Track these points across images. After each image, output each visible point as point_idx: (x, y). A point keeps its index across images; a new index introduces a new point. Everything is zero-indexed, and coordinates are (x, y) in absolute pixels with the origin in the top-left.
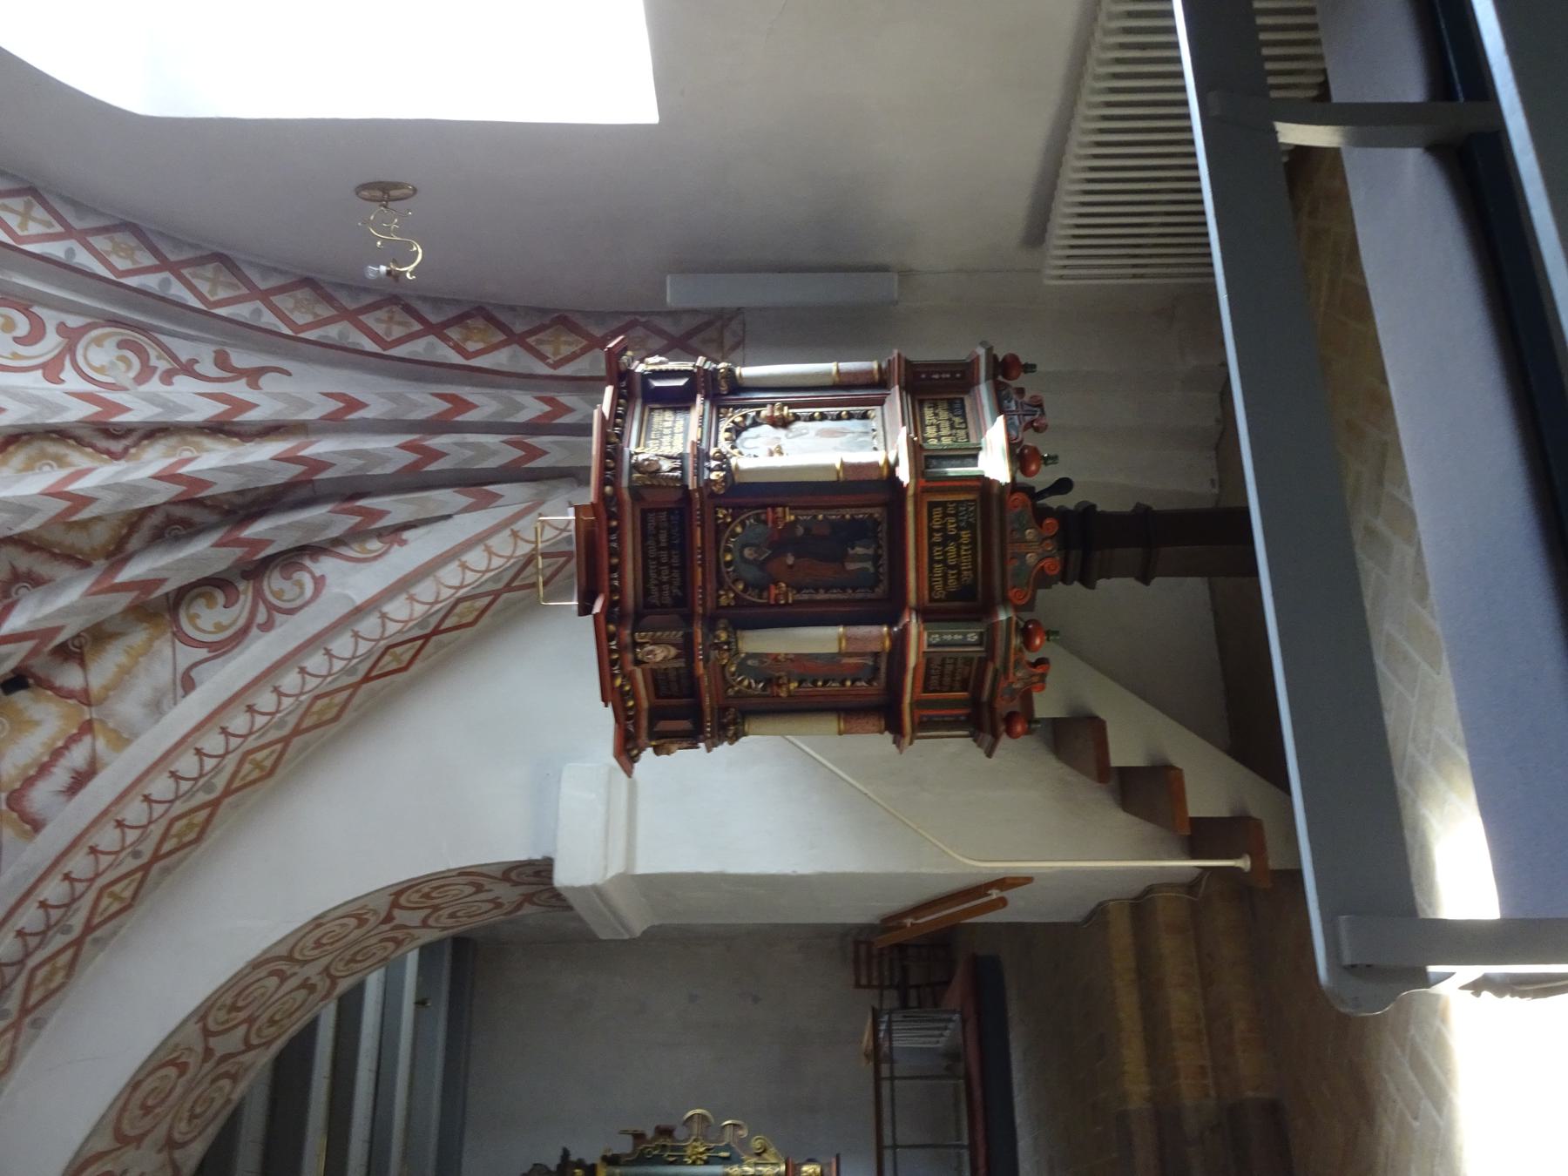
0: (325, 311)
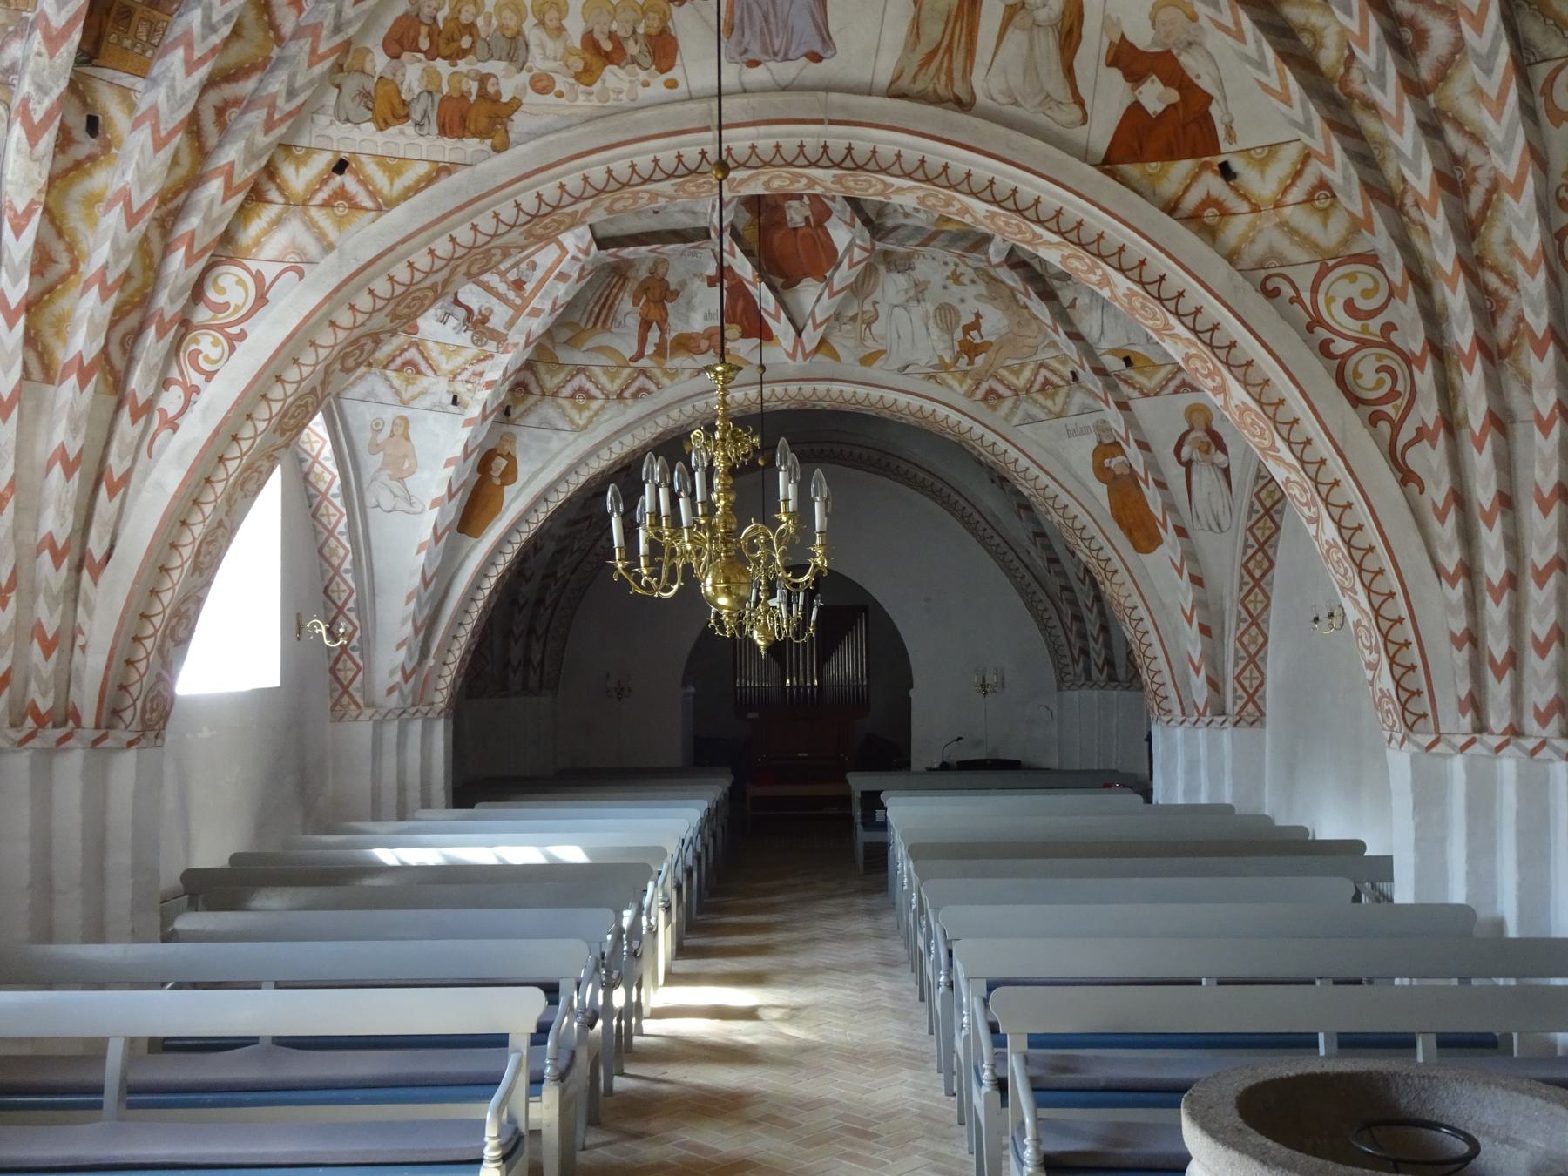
0: (333, 542)
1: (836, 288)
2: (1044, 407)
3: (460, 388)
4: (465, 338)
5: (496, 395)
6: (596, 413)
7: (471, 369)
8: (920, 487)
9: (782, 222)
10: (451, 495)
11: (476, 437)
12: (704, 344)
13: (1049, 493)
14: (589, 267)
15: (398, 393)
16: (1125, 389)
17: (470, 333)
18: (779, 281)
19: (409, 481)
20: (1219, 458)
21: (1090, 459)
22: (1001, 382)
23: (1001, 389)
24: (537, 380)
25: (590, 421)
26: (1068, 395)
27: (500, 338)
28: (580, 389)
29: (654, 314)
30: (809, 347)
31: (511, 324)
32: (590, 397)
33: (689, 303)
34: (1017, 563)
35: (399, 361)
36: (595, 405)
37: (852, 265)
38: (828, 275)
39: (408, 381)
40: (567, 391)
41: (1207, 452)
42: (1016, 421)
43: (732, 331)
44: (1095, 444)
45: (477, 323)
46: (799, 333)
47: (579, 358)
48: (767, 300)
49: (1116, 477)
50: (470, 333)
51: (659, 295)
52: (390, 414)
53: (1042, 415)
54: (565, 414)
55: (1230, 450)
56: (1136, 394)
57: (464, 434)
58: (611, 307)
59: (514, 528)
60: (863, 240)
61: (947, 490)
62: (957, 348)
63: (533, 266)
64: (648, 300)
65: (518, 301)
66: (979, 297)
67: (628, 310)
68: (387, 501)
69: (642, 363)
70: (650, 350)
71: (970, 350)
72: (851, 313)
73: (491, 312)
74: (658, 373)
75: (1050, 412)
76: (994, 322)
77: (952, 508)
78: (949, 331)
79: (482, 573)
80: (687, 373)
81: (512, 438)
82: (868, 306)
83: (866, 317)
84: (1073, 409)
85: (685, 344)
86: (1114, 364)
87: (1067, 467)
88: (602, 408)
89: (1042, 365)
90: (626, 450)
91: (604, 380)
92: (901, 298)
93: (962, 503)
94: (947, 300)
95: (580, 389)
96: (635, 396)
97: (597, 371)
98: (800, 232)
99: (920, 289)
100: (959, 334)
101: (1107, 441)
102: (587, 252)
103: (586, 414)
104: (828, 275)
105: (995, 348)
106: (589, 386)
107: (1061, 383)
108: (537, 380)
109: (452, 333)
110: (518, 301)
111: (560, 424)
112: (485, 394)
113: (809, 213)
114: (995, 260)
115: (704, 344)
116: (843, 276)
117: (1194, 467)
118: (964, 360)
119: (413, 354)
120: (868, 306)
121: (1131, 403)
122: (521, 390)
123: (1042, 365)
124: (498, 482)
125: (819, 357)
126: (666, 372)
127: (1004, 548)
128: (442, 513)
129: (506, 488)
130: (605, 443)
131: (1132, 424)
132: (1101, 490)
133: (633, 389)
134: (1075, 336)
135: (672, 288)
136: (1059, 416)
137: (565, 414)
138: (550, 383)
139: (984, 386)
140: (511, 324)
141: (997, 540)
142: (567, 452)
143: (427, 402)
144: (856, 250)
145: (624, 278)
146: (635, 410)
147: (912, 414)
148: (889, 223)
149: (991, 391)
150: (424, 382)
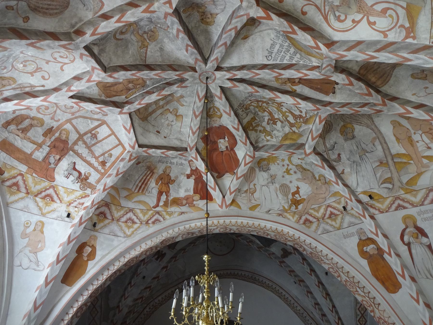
1: (239, 176)
2: (331, 225)
3: (72, 210)
4: (77, 186)
5: (87, 213)
6: (136, 230)
7: (78, 201)
8: (268, 287)
9: (217, 149)
10: (58, 261)
11: (75, 233)
12: (184, 202)
13: (339, 265)
14: (134, 155)
15: (40, 209)
16: (372, 210)
17: (79, 184)
18: (216, 175)
19: (39, 254)
20: (424, 240)
21: (357, 248)
22: (311, 215)
23: (311, 219)
24: (111, 212)
25: (133, 233)
26: (342, 219)
27: (93, 188)
28: (130, 219)
29: (164, 189)
30: (228, 202)
31: (98, 181)
32: (134, 222)
33: (179, 185)
34: (308, 318)
35: (43, 194)
36: (136, 226)
37: (246, 165)
38: (235, 171)
39: (47, 204)
40: (124, 219)
41: (417, 238)
42: (319, 232)
43: (197, 197)
45: (83, 179)
46: (224, 197)
47: (131, 205)
48: (210, 180)
49: (371, 256)
50: (79, 184)
51: (166, 181)
52: (34, 219)
53: (331, 229)
54: (122, 229)
56: (377, 212)
57: (70, 231)
58: (146, 184)
59: (90, 282)
60: (250, 152)
61: (278, 288)
62: (290, 203)
63: (111, 156)
64: (162, 183)
65: (103, 171)
66: (298, 180)
67: (153, 187)
68: (26, 263)
69: (158, 209)
70: (161, 204)
71: (296, 203)
72: (245, 189)
73: (90, 175)
74: (164, 213)
75: (334, 227)
76: (305, 190)
77: (280, 296)
78: (286, 195)
79: (69, 305)
80: (176, 214)
81: (95, 238)
82: (252, 186)
83: (251, 190)
84: (345, 225)
85: (177, 202)
86: (365, 199)
87: (346, 253)
88: (139, 227)
89: (328, 206)
90: (148, 247)
91: (141, 215)
92: (265, 182)
93: (284, 293)
94: (284, 182)
95: (130, 219)
96: (154, 223)
97: (138, 211)
98: (224, 153)
99: (273, 179)
100: (290, 196)
102: (133, 148)
103: (131, 230)
104: (235, 171)
105: (305, 203)
106: (134, 218)
107: (338, 213)
108: (111, 212)
109: (71, 183)
110: (103, 171)
111: (119, 234)
112: (82, 212)
113: (227, 145)
114: (308, 151)
115: (184, 202)
116: (242, 170)
117: (412, 246)
118: (293, 207)
119: (51, 191)
120: (252, 186)
121: (375, 216)
122: (100, 216)
123: (328, 206)
124: (86, 259)
125: (232, 207)
126: (167, 213)
127: (302, 311)
128: (51, 270)
129: (90, 262)
130: (138, 243)
131: (378, 226)
132: (364, 263)
133: (153, 219)
134: (346, 185)
135: (172, 179)
136: (339, 229)
137: (122, 229)
138: (117, 215)
139: (303, 218)
140: (98, 181)
141: (299, 308)
142: (120, 246)
143: (54, 215)
144: (247, 157)
145: (152, 172)
146: (152, 229)
147: (273, 232)
148: (260, 145)
149: (307, 220)
150: (54, 206)
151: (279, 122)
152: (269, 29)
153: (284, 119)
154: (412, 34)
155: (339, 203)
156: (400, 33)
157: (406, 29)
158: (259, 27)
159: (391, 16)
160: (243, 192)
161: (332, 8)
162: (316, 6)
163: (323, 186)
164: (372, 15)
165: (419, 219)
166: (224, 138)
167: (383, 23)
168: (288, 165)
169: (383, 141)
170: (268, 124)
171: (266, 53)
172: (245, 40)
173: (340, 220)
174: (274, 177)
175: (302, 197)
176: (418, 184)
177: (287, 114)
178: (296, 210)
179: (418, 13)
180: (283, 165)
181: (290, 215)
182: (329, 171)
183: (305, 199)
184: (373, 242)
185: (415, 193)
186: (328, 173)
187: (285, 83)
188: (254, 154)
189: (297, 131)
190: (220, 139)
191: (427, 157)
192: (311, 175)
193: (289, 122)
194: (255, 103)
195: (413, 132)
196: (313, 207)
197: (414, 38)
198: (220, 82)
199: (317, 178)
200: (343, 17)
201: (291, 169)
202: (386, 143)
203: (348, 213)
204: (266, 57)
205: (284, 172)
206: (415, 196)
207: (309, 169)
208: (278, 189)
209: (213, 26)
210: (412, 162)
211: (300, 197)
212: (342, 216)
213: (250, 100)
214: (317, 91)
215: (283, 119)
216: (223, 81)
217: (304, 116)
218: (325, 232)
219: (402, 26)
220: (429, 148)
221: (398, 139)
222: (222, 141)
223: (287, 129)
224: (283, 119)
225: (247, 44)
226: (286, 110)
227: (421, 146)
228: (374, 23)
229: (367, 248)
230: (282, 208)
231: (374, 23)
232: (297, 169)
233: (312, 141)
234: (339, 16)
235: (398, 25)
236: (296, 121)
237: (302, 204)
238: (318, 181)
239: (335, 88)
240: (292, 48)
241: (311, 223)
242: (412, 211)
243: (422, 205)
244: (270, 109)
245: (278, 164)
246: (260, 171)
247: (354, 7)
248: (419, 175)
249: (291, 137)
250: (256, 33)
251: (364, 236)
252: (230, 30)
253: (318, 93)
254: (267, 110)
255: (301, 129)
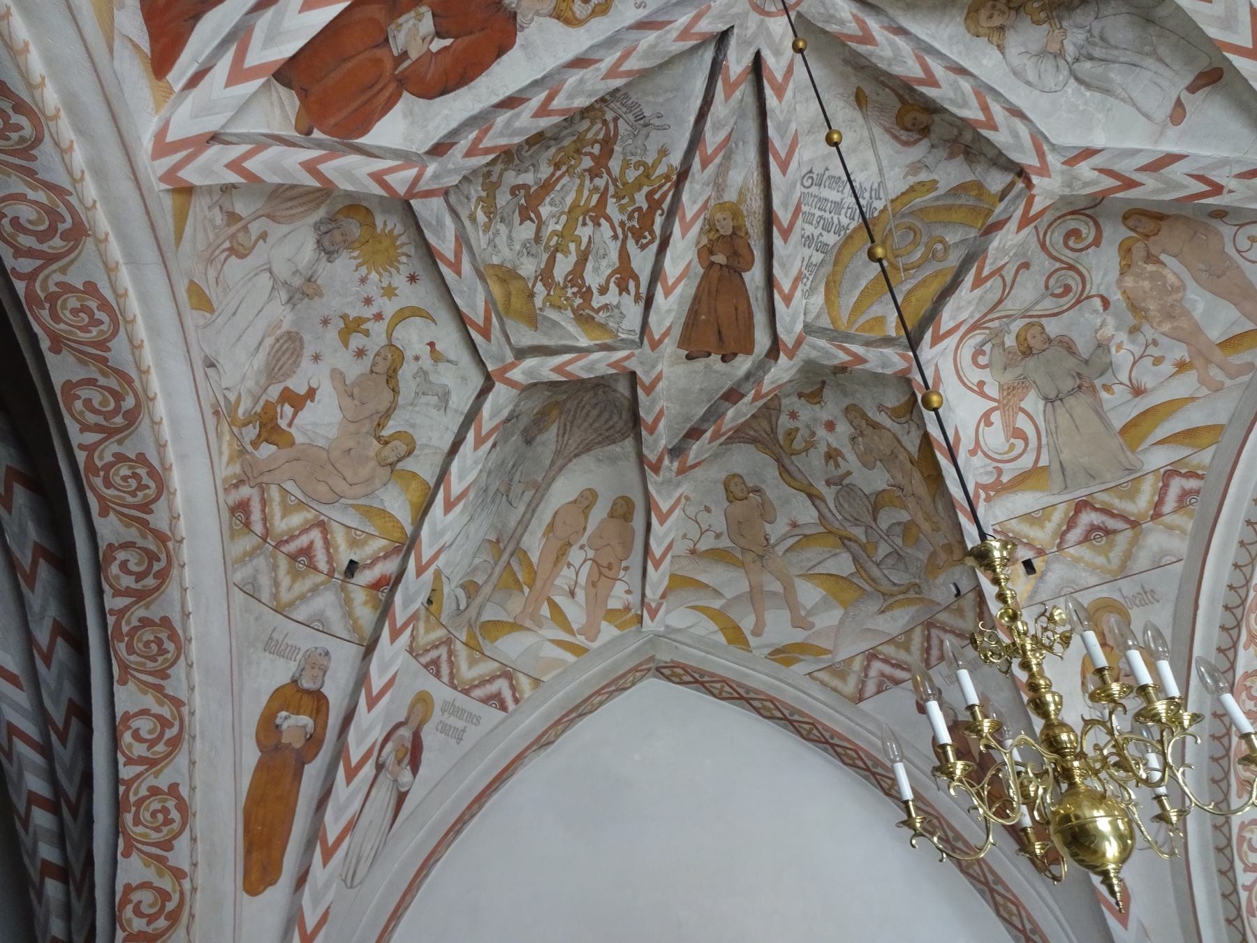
2: (276, 584)
21: (264, 700)
22: (264, 503)
23: (256, 516)
26: (315, 590)
44: (286, 679)
49: (278, 747)
53: (265, 596)
55: (422, 770)
60: (436, 176)
62: (258, 409)
66: (337, 375)
75: (275, 596)
76: (321, 421)
84: (302, 613)
89: (322, 525)
94: (307, 338)
95: (1094, 528)
98: (379, 53)
99: (304, 290)
100: (274, 392)
101: (306, 684)
104: (317, 134)
105: (286, 453)
113: (414, 55)
118: (251, 432)
151: (534, 226)
152: (881, 170)
153: (553, 243)
154: (992, 493)
155: (354, 543)
156: (987, 473)
157: (998, 480)
158: (887, 137)
159: (1012, 447)
160: (227, 206)
161: (997, 335)
162: (1000, 301)
163: (372, 464)
164: (1003, 415)
165: (437, 716)
166: (439, 34)
167: (995, 438)
168: (379, 317)
169: (533, 506)
170: (514, 190)
171: (818, 170)
172: (853, 98)
173: (306, 588)
174: (310, 291)
175: (293, 431)
176: (496, 644)
177: (572, 246)
178: (249, 448)
179: (1034, 489)
180: (368, 301)
181: (230, 444)
182: (476, 462)
183: (293, 444)
184: (318, 711)
185: (477, 655)
186: (469, 462)
187: (710, 231)
188: (429, 194)
189: (538, 302)
190: (434, 15)
191: (553, 606)
192: (383, 407)
193: (552, 261)
194: (597, 134)
195: (584, 540)
196: (289, 486)
197: (988, 499)
198: (749, 32)
199: (386, 433)
200: (982, 360)
201: (367, 333)
202: (534, 511)
203: (343, 589)
204: (811, 171)
205: (344, 317)
206: (472, 663)
207: (402, 390)
208: (279, 332)
209: (962, 29)
210: (526, 590)
211: (290, 425)
212: (322, 583)
213: (616, 120)
214: (688, 317)
215: (550, 239)
216: (750, 44)
217: (595, 305)
218: (249, 588)
219: (1000, 472)
220: (572, 594)
221: (551, 526)
222: (427, 24)
223: (528, 268)
224: (550, 239)
225: (842, 104)
226: (585, 241)
227: (565, 577)
228: (989, 424)
229: (286, 718)
230: (232, 397)
231: (989, 424)
232: (377, 354)
233: (552, 370)
234: (983, 353)
235: (1000, 465)
236: (565, 287)
237: (274, 448)
238: (379, 439)
239: (709, 355)
240: (837, 238)
241: (246, 530)
242: (441, 692)
243: (466, 692)
244: (563, 181)
245: (363, 280)
246: (316, 226)
247: (1008, 377)
248: (515, 627)
249: (514, 292)
250: (870, 129)
251: (314, 678)
252: (985, 109)
253: (683, 320)
254: (558, 173)
255: (552, 314)
